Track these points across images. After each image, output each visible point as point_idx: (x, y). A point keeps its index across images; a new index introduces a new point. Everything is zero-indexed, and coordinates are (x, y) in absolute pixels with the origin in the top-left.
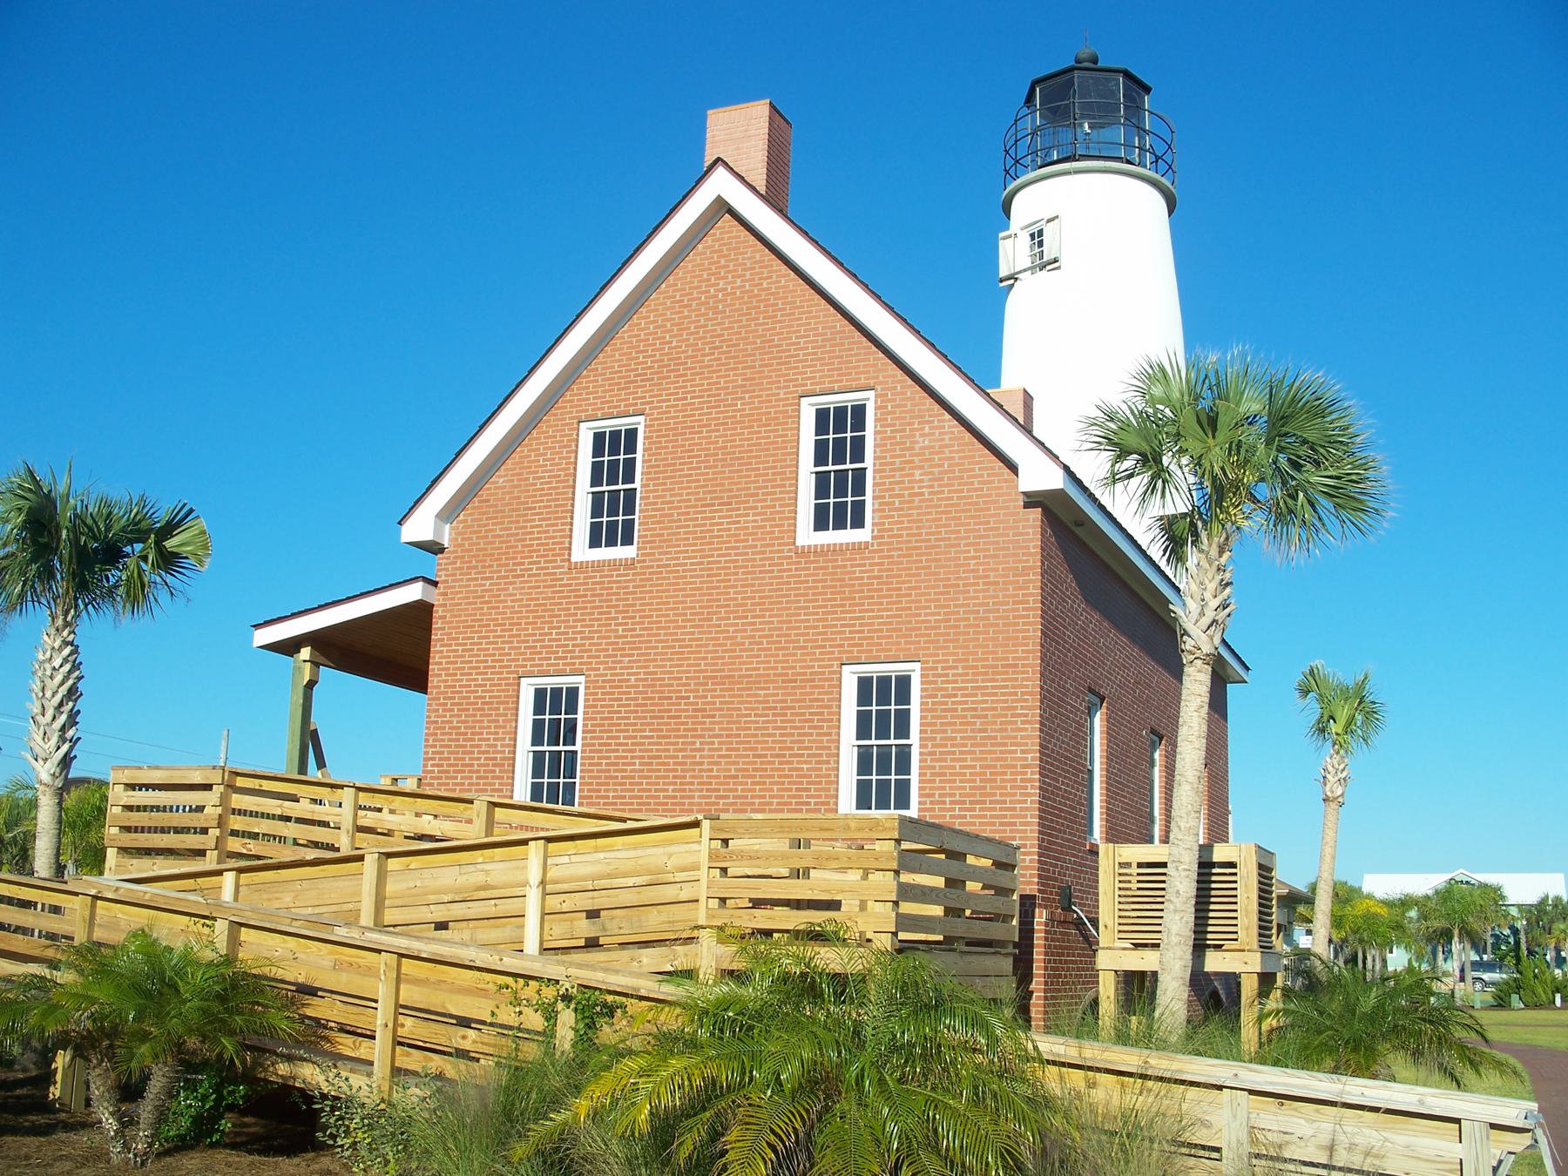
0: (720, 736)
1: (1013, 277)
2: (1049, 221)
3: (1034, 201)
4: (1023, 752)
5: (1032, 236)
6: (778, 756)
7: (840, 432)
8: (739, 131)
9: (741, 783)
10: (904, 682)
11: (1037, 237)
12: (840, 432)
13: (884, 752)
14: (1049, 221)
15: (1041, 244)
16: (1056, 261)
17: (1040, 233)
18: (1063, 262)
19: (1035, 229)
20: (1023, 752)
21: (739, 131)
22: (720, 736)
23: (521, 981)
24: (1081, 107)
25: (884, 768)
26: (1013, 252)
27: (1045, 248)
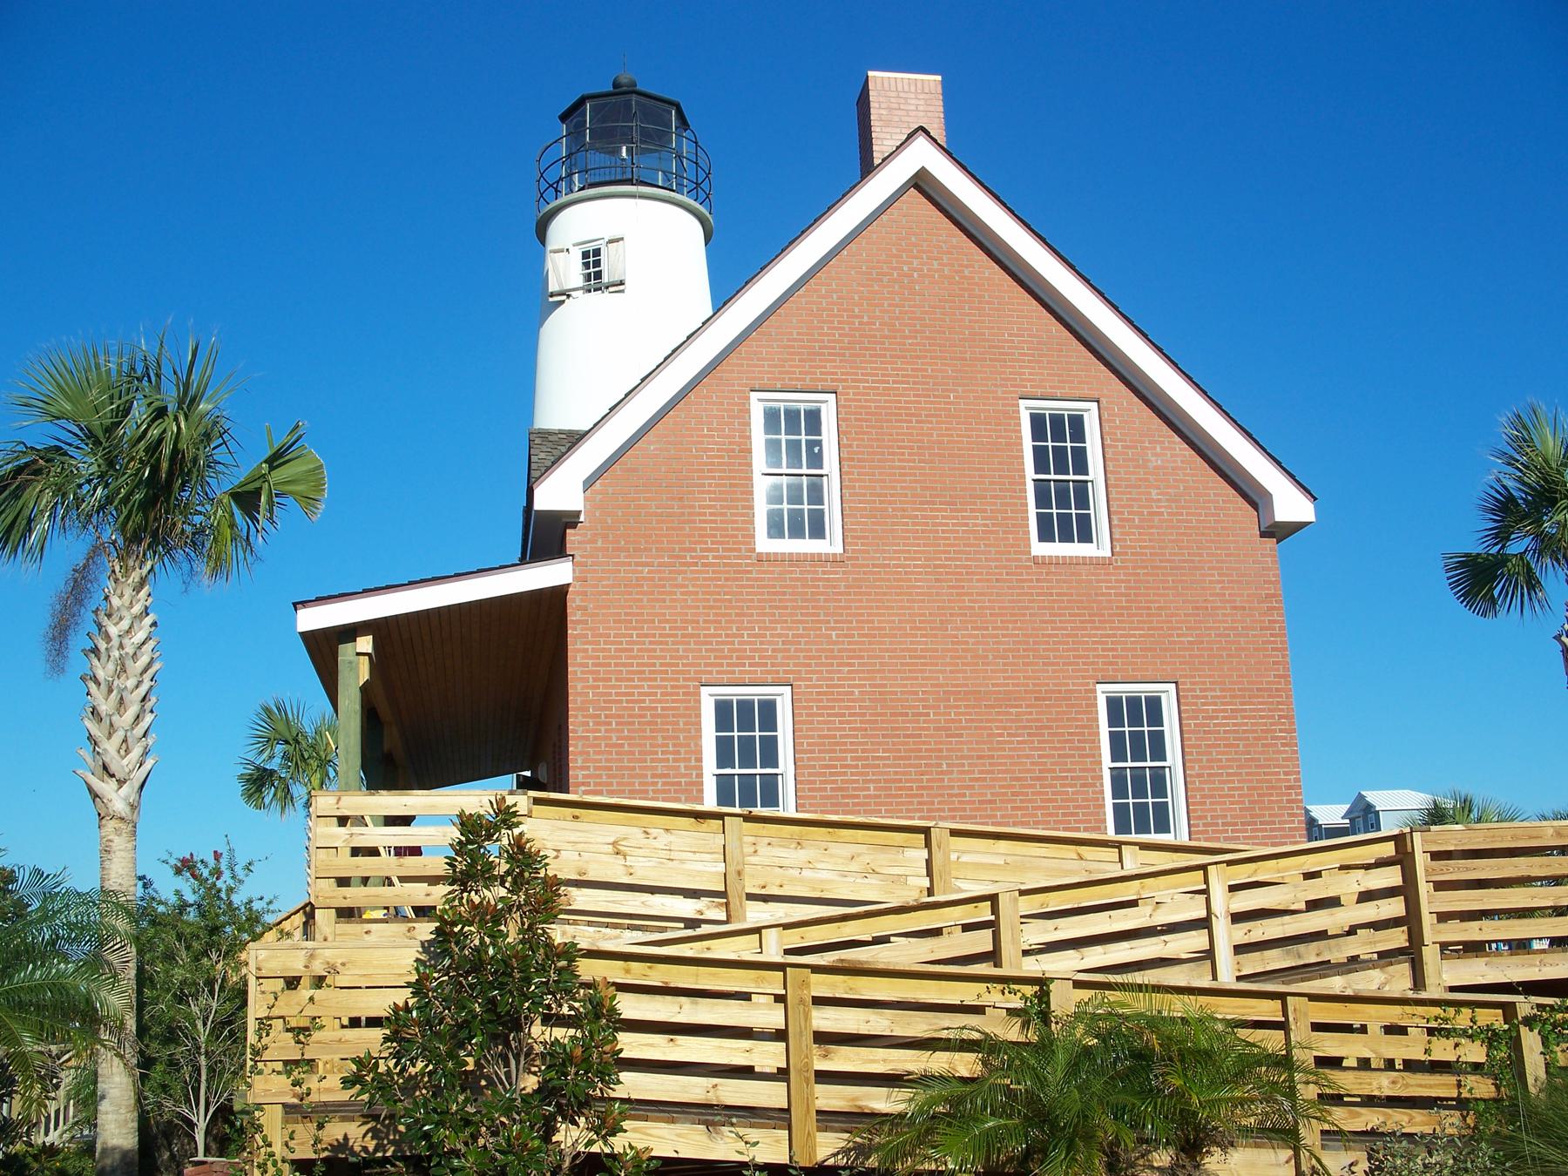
0: (971, 757)
1: (566, 294)
2: (611, 241)
3: (581, 222)
4: (1286, 774)
5: (585, 255)
6: (1038, 779)
7: (1059, 440)
8: (905, 98)
9: (1000, 809)
10: (769, 708)
11: (592, 259)
12: (1059, 440)
13: (1138, 774)
14: (611, 241)
15: (597, 263)
16: (622, 283)
17: (597, 252)
18: (627, 286)
19: (591, 247)
20: (1286, 774)
21: (905, 98)
22: (971, 757)
23: (1451, 1010)
24: (622, 132)
25: (1140, 791)
26: (564, 270)
27: (604, 267)
